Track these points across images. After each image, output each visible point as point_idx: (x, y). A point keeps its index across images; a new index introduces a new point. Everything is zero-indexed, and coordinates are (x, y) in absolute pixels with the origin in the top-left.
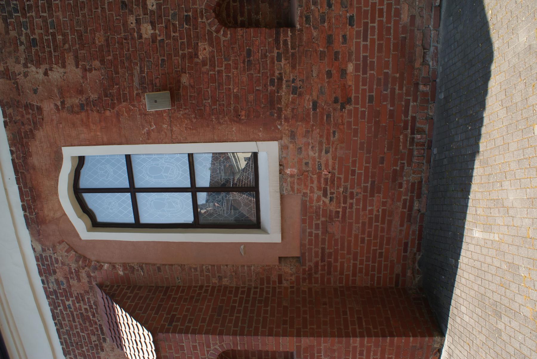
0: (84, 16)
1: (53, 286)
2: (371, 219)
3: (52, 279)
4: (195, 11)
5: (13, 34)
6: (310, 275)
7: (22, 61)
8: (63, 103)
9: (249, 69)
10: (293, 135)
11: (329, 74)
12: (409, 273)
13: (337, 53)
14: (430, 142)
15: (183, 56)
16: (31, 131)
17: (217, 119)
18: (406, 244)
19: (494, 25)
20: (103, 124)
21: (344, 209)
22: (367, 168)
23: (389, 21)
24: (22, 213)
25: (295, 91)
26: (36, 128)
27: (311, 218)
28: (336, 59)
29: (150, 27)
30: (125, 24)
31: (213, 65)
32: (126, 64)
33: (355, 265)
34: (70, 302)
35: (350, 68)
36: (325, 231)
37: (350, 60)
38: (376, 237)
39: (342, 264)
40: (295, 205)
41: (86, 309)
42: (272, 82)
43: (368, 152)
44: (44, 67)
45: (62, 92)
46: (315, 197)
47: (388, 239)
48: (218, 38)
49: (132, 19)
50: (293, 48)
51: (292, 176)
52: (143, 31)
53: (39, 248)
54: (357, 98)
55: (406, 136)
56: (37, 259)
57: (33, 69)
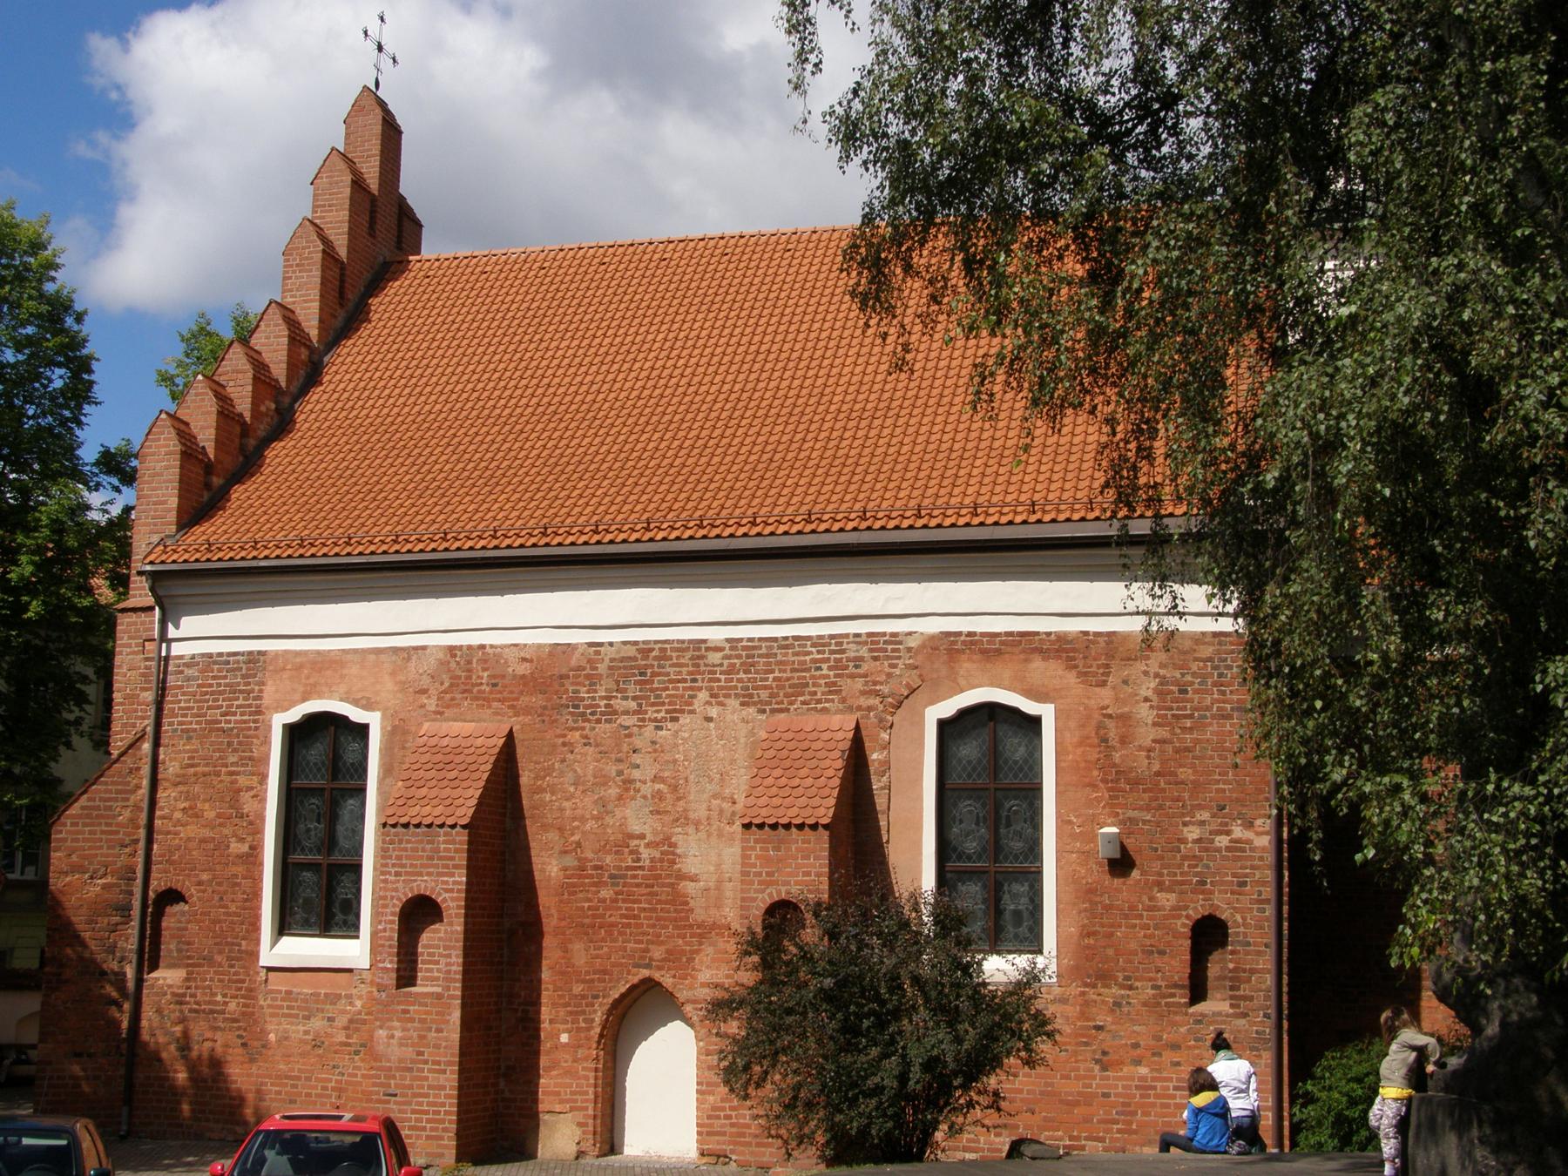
0: (1212, 758)
1: (852, 651)
3: (864, 652)
4: (1212, 892)
5: (1194, 667)
7: (1162, 672)
8: (1110, 716)
9: (1143, 952)
11: (1136, 1046)
13: (1160, 1055)
15: (1160, 874)
16: (1076, 667)
17: (1085, 910)
20: (1083, 765)
25: (1117, 1004)
26: (1081, 674)
28: (1154, 1054)
29: (1196, 836)
30: (1200, 807)
31: (1150, 909)
32: (1154, 804)
34: (825, 672)
35: (1143, 1071)
37: (1152, 1070)
41: (815, 693)
42: (1127, 978)
43: (1042, 1093)
44: (1155, 698)
45: (1124, 719)
48: (1179, 917)
49: (1206, 815)
50: (1167, 1004)
52: (1191, 828)
53: (913, 643)
54: (1108, 1078)
55: (1061, 1139)
57: (1152, 685)
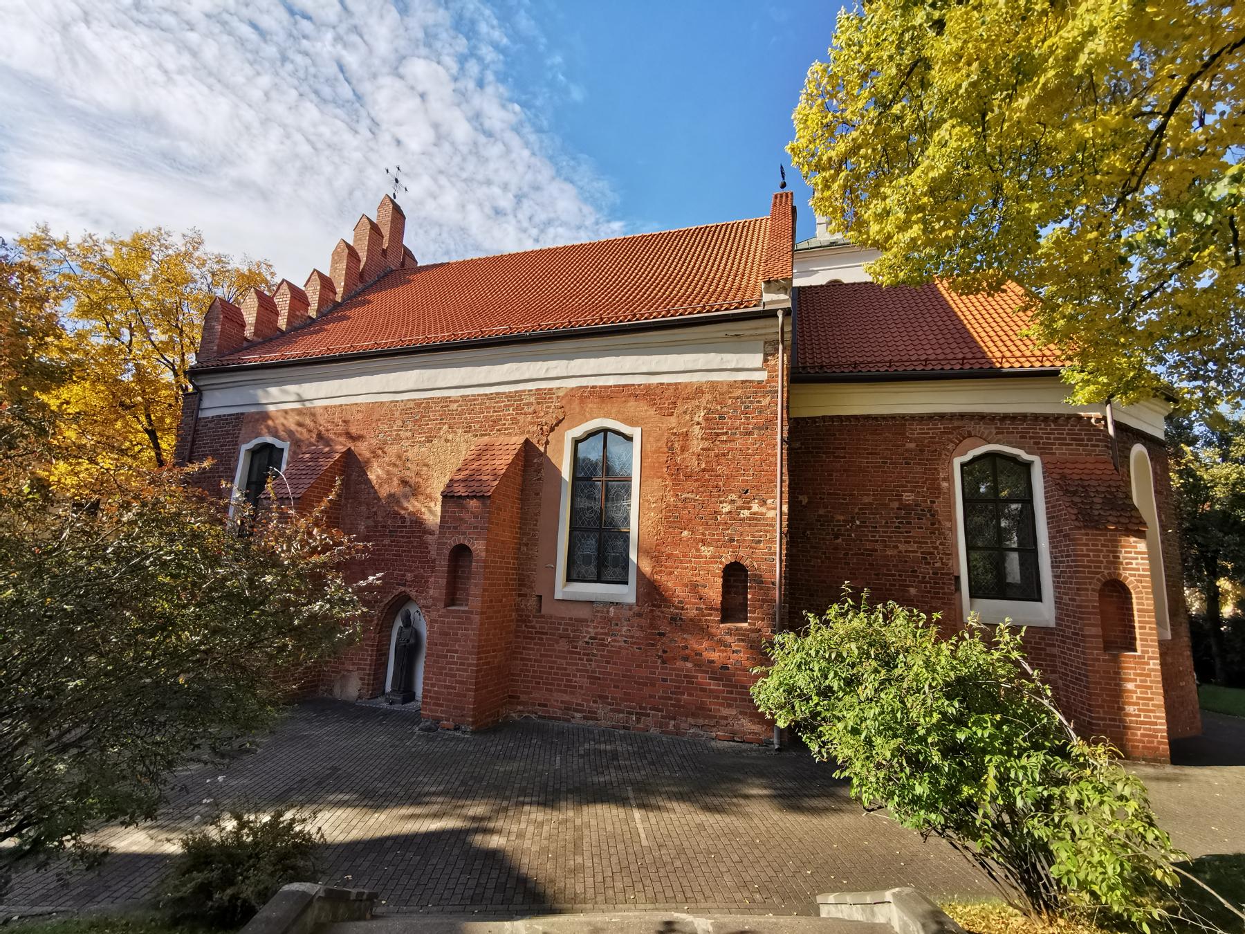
2: (569, 675)
6: (525, 621)
10: (639, 615)
12: (520, 708)
14: (628, 728)
15: (703, 534)
18: (545, 706)
19: (447, 253)
21: (579, 653)
22: (610, 674)
24: (591, 384)
27: (573, 625)
30: (731, 491)
33: (530, 660)
39: (533, 649)
40: (584, 613)
47: (551, 690)
49: (733, 497)
51: (608, 612)
56: (551, 389)
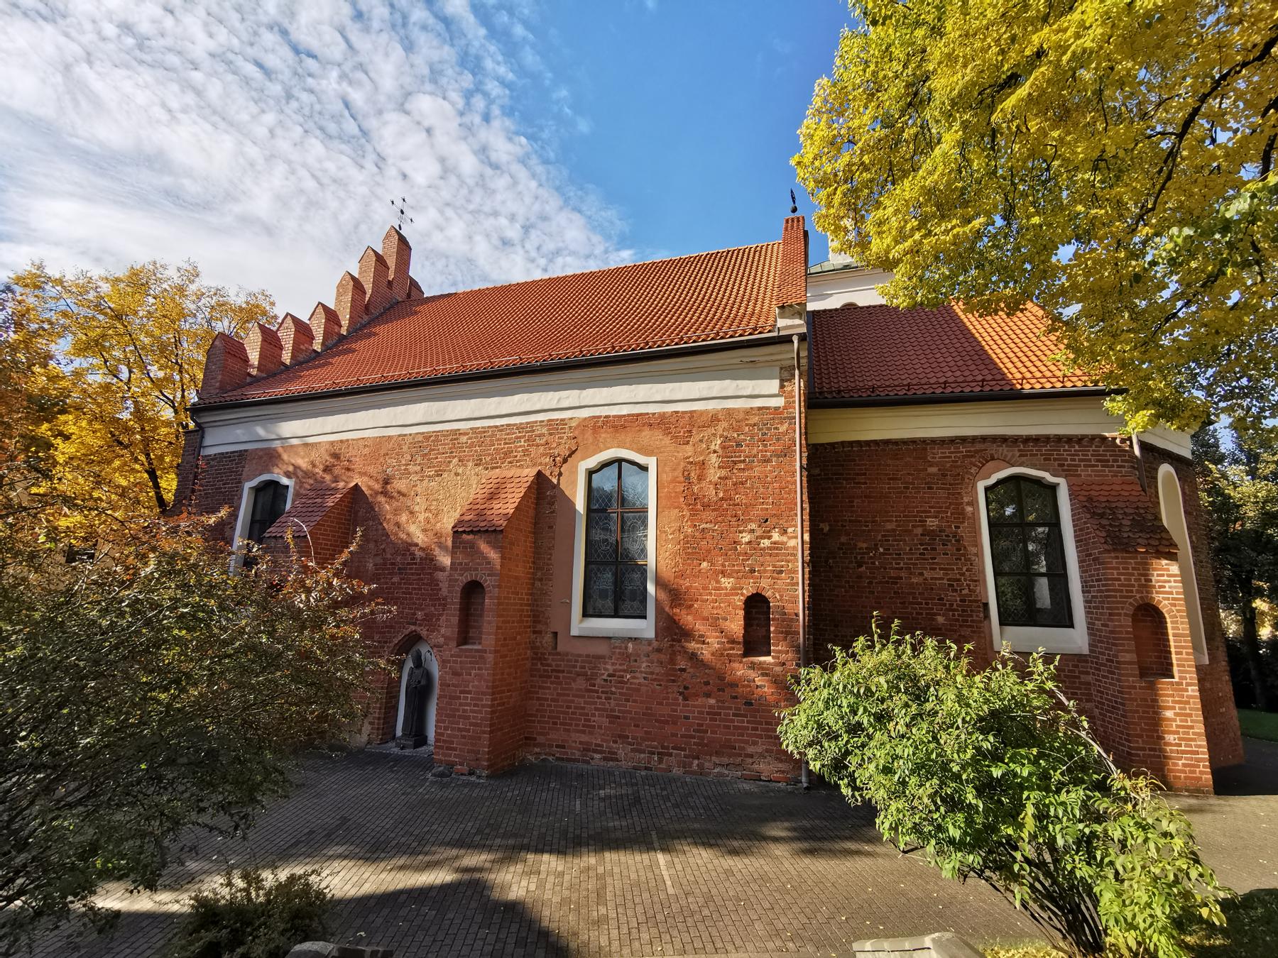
3: (544, 430)
6: (540, 659)
10: (659, 650)
11: (707, 683)
14: (650, 769)
15: (723, 565)
18: (563, 747)
21: (597, 692)
22: (630, 712)
23: (748, 735)
24: (604, 414)
28: (719, 690)
30: (751, 521)
33: (547, 699)
35: (712, 701)
36: (578, 674)
38: (571, 719)
39: (549, 688)
40: (602, 649)
46: (609, 667)
47: (568, 730)
49: (753, 526)
51: (626, 648)
